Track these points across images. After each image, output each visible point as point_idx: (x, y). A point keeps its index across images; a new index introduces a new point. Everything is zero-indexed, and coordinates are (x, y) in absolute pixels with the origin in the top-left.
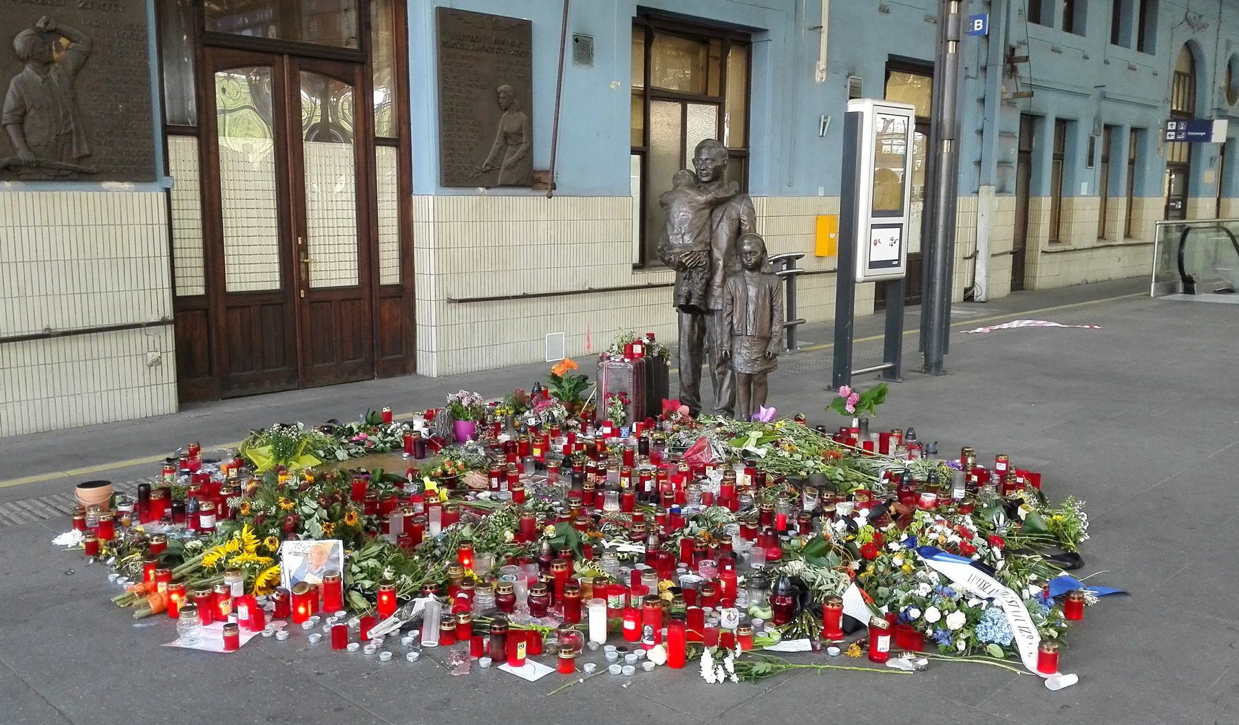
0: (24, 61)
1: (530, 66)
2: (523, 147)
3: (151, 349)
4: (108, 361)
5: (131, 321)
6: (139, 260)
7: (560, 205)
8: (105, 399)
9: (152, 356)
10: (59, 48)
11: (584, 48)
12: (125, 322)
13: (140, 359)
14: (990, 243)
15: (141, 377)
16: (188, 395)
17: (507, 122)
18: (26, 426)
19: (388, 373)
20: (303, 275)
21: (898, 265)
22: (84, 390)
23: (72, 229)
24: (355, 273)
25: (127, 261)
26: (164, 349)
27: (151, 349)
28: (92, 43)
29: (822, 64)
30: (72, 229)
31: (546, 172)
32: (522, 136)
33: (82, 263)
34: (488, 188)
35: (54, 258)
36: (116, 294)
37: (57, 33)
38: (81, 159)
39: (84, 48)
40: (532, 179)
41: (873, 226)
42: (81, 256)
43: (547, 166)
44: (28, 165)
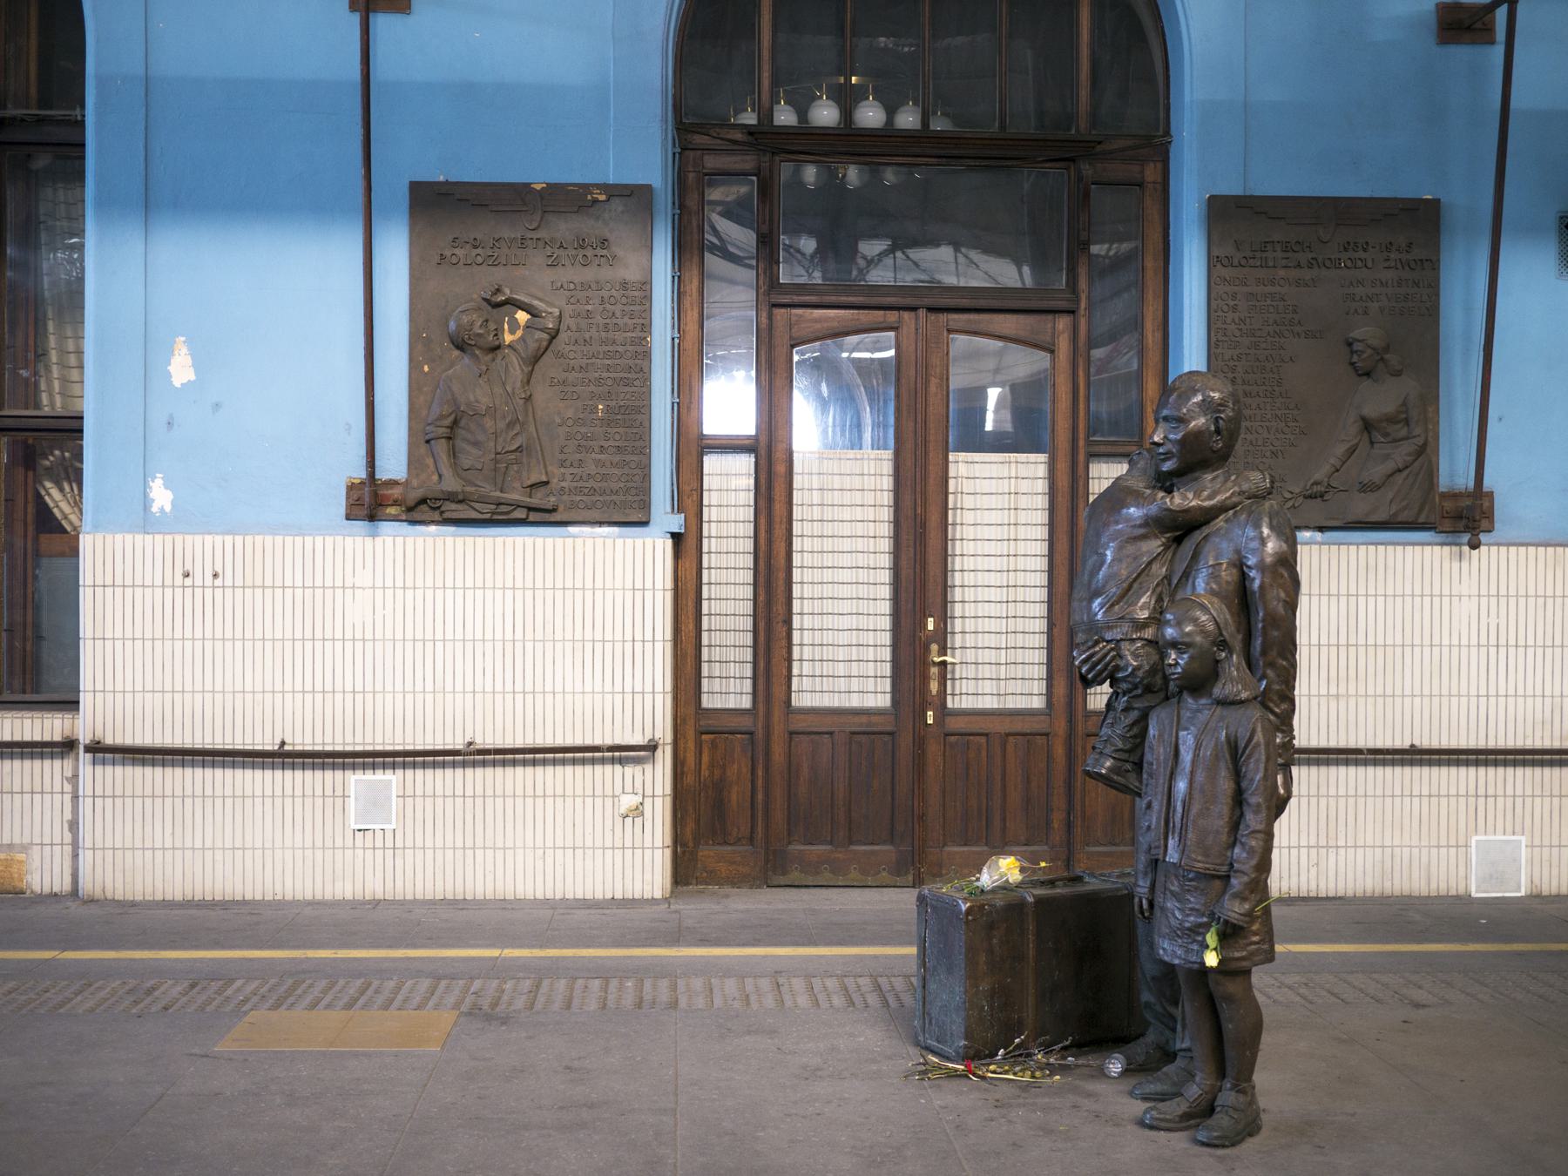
3: (628, 788)
4: (559, 801)
6: (618, 646)
7: (1492, 562)
8: (549, 860)
9: (629, 801)
10: (514, 325)
13: (609, 801)
15: (608, 834)
16: (685, 870)
20: (934, 687)
22: (519, 844)
23: (519, 593)
24: (1039, 687)
25: (598, 646)
26: (649, 792)
27: (628, 788)
30: (519, 593)
32: (1413, 428)
33: (529, 645)
35: (489, 636)
36: (259, 697)
40: (1466, 519)
42: (529, 636)
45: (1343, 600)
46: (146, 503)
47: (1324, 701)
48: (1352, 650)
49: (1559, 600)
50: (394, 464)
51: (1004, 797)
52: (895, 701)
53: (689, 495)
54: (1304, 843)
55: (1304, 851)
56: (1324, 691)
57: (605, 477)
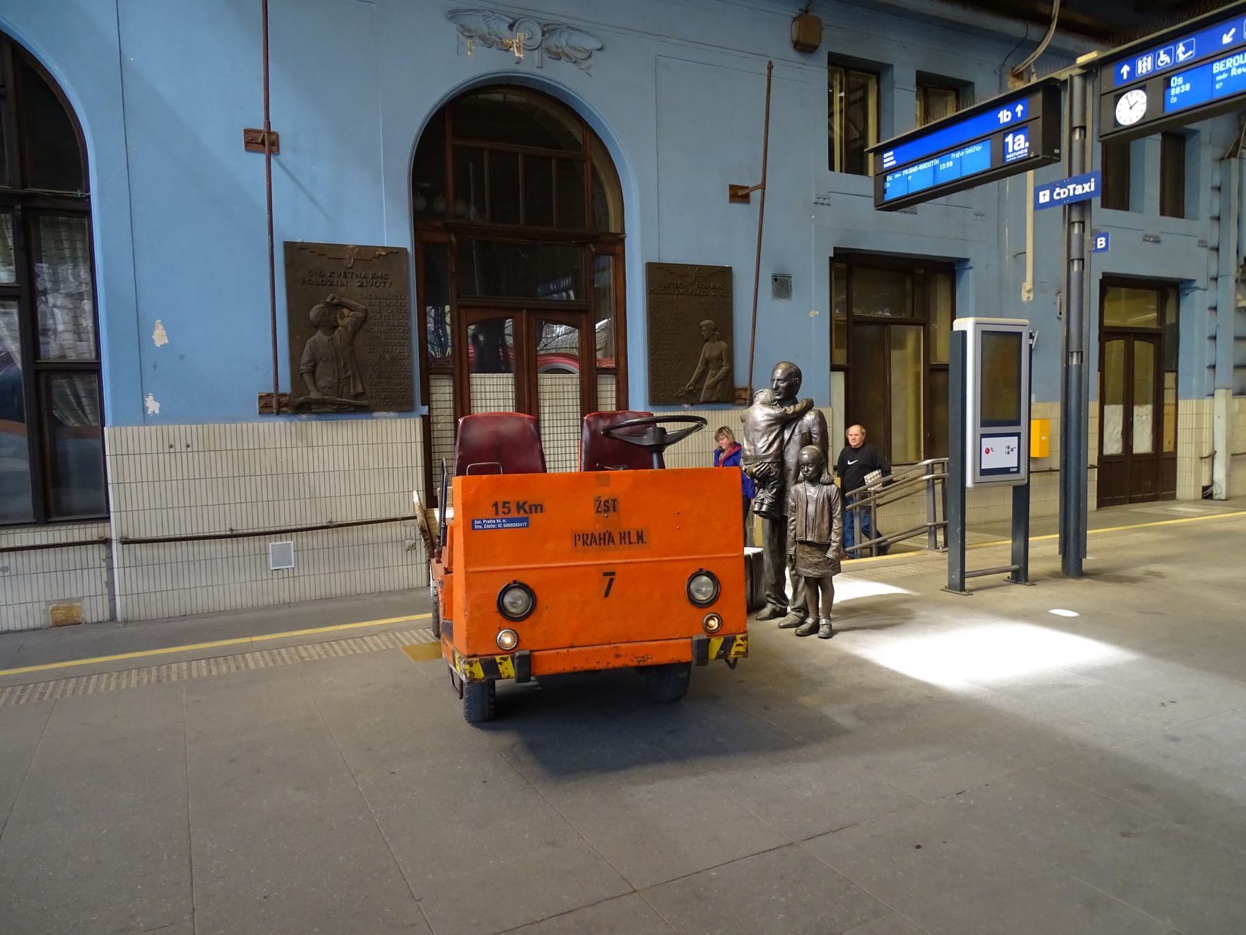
0: (317, 327)
1: (731, 303)
2: (723, 370)
5: (393, 516)
11: (782, 285)
12: (388, 517)
14: (1229, 443)
17: (710, 350)
18: (160, 613)
19: (1164, 498)
21: (1018, 471)
28: (366, 311)
29: (1028, 285)
31: (745, 390)
34: (692, 405)
37: (340, 305)
38: (357, 396)
39: (361, 314)
41: (983, 436)
43: (746, 385)
44: (316, 402)
46: (144, 409)
53: (426, 400)
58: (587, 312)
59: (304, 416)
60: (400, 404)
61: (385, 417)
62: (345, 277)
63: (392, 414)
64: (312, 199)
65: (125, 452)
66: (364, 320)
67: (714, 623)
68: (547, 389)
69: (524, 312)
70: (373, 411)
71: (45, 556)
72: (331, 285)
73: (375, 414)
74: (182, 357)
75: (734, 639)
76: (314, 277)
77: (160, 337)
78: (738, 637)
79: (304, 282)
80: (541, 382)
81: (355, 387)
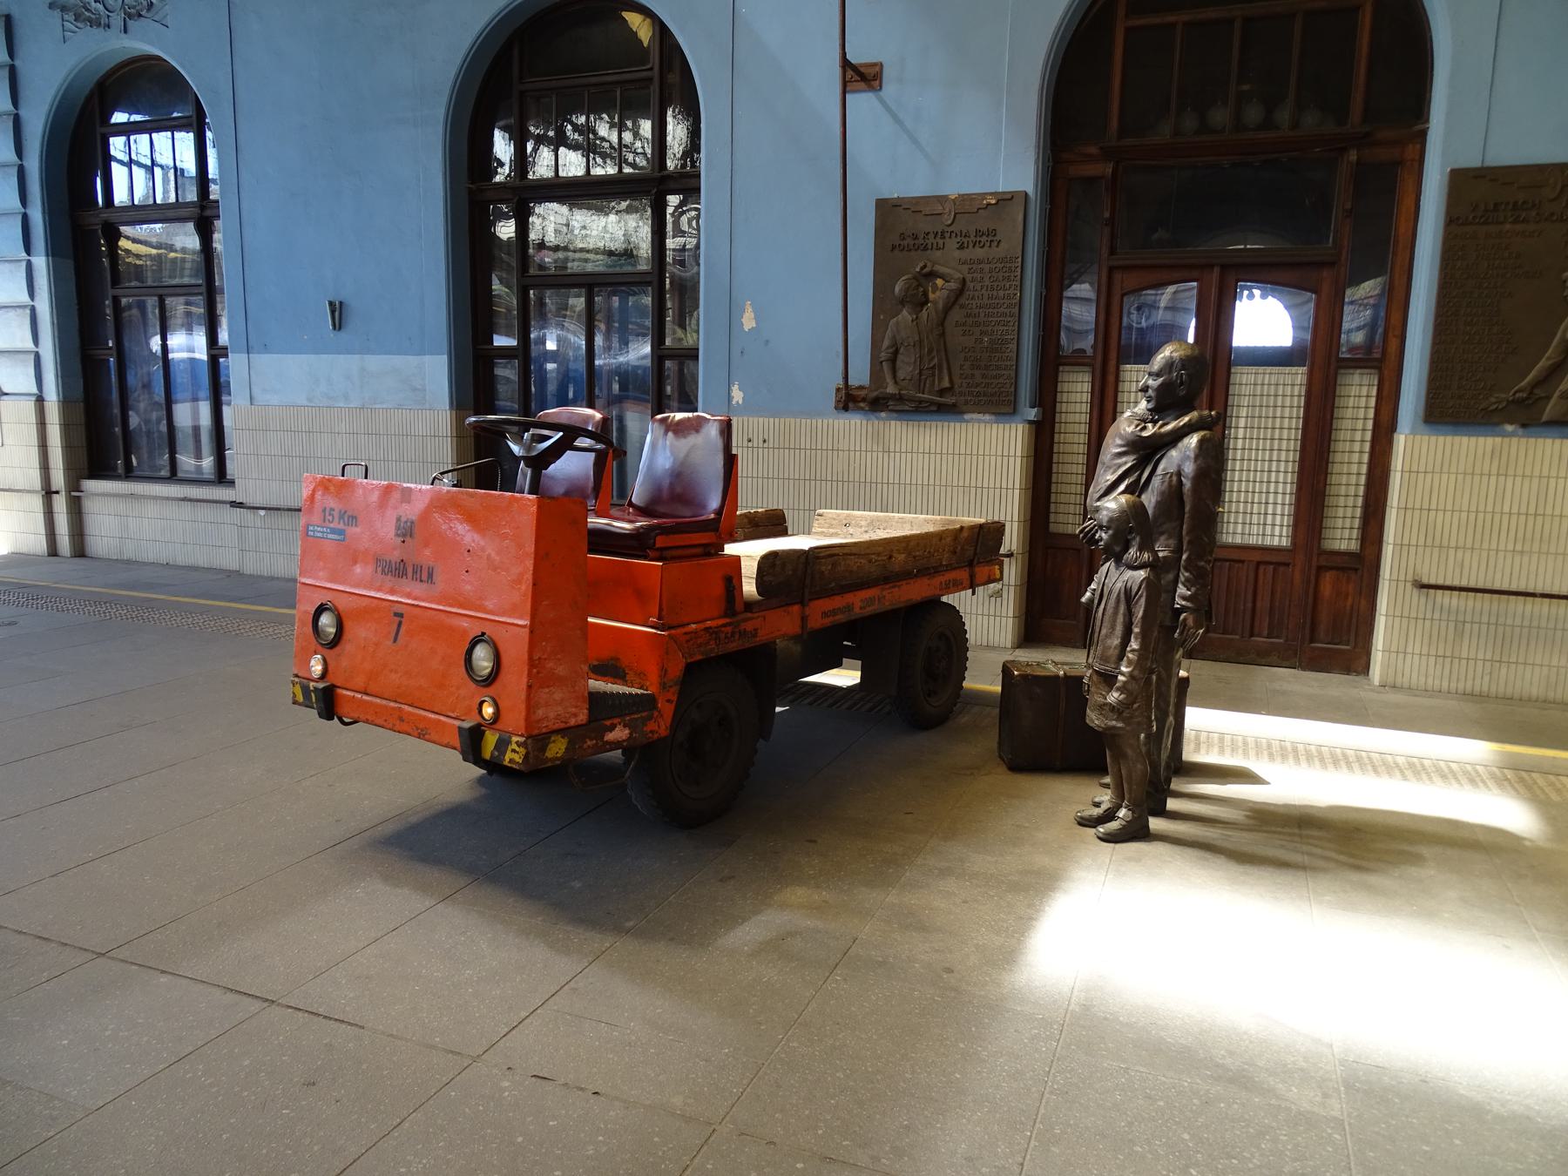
0: (902, 302)
10: (935, 288)
34: (1524, 426)
37: (932, 275)
38: (942, 392)
39: (953, 285)
44: (892, 397)
45: (1535, 481)
46: (730, 398)
47: (1509, 556)
48: (1540, 519)
49: (1559, 633)
50: (860, 375)
51: (1254, 602)
52: (1294, 543)
53: (1047, 398)
54: (1481, 656)
55: (1480, 663)
56: (1510, 547)
57: (988, 385)
58: (1332, 264)
59: (883, 414)
60: (1000, 405)
61: (979, 421)
62: (943, 237)
63: (987, 417)
64: (915, 141)
65: (1422, 469)
66: (960, 292)
67: (488, 711)
68: (1246, 390)
69: (1217, 270)
70: (963, 413)
71: (1495, 604)
72: (925, 249)
73: (967, 417)
74: (767, 342)
75: (509, 742)
76: (909, 239)
77: (748, 321)
78: (515, 739)
79: (894, 248)
80: (1235, 378)
81: (941, 379)
